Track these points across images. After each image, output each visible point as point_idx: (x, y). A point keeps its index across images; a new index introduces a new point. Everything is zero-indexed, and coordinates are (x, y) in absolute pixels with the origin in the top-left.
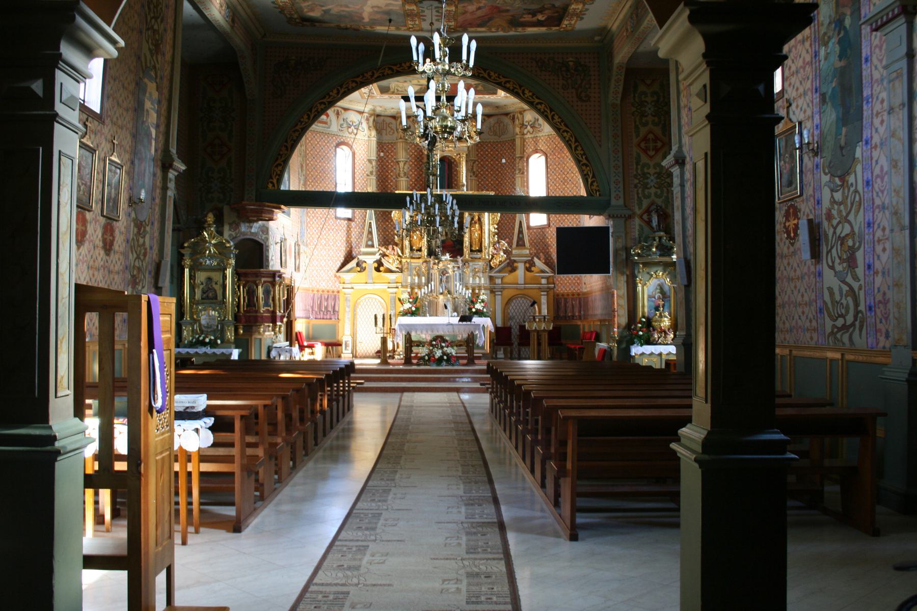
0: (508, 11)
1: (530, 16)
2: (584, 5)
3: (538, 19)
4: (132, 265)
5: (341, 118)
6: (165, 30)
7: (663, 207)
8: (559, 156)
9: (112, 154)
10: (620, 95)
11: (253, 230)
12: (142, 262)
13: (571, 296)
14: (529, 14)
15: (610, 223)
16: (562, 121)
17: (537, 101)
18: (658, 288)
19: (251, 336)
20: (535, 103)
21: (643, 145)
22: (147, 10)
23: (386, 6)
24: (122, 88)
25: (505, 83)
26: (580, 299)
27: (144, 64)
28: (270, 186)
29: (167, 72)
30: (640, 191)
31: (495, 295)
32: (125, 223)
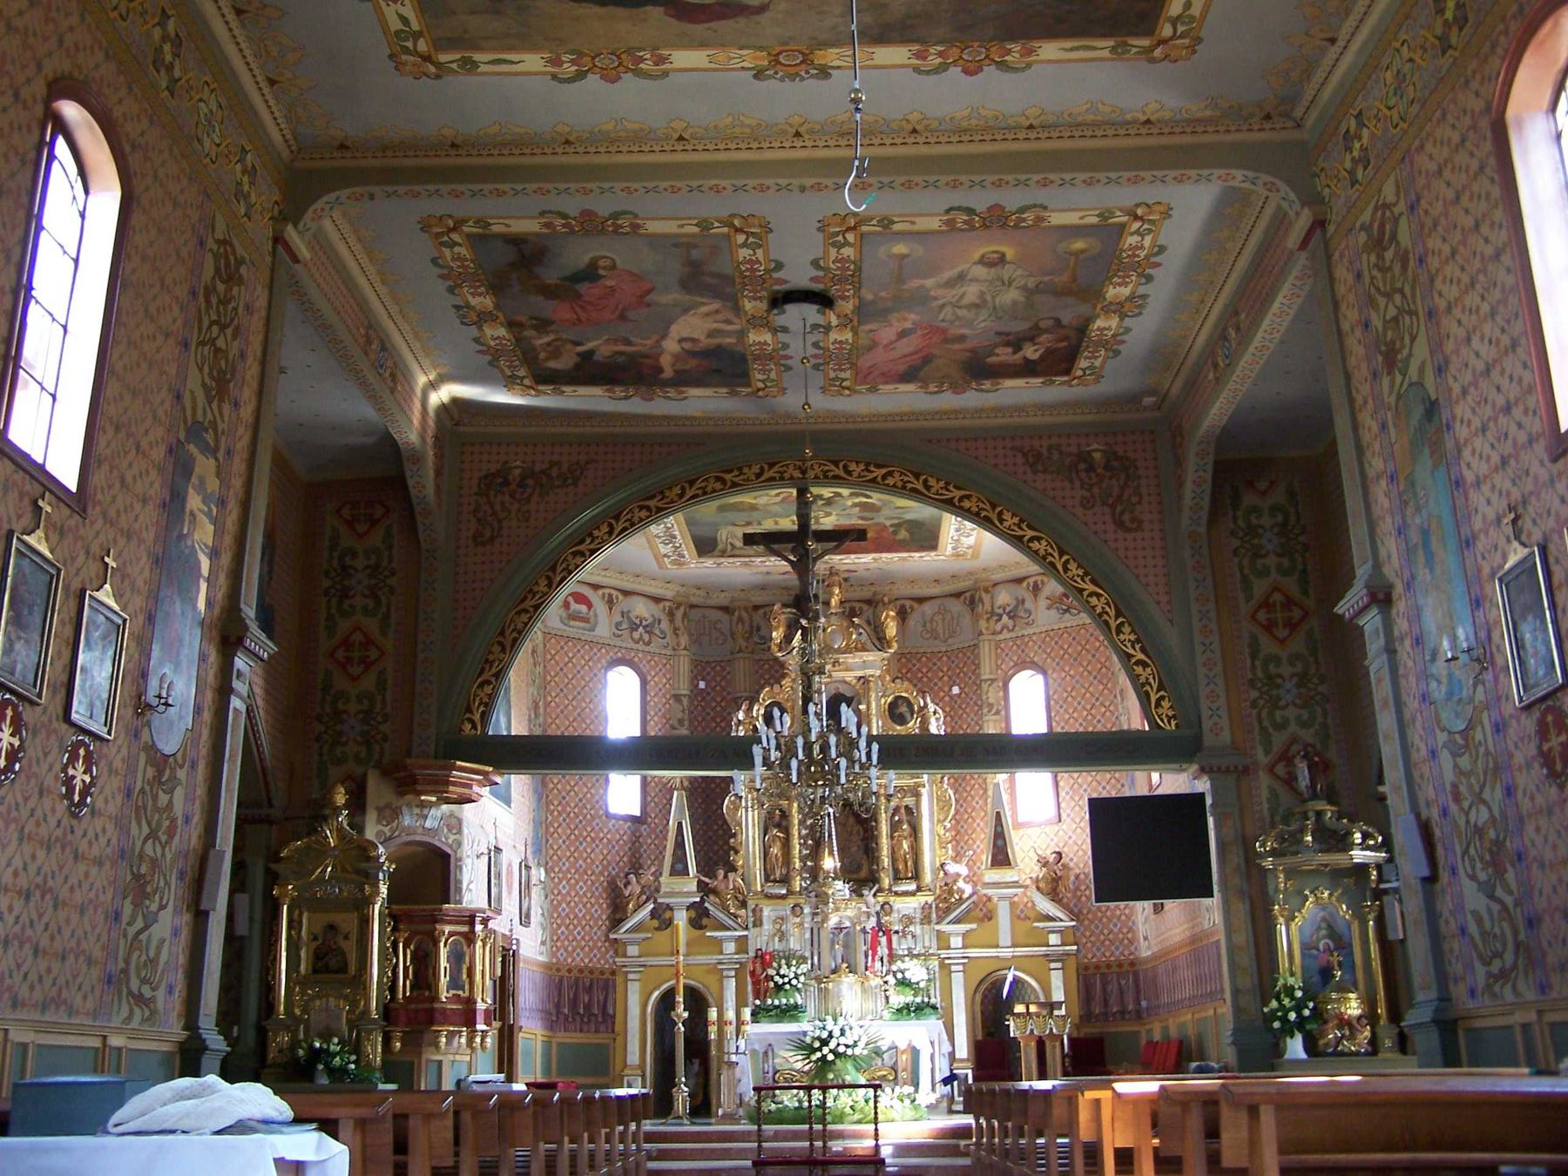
0: (962, 338)
1: (1010, 350)
2: (1122, 320)
3: (1025, 358)
4: (137, 850)
5: (617, 609)
6: (242, 355)
7: (1318, 746)
8: (1072, 672)
9: (101, 587)
10: (1205, 514)
11: (428, 824)
12: (163, 848)
13: (1115, 969)
14: (1008, 344)
15: (1203, 785)
16: (1086, 574)
17: (1030, 533)
18: (1324, 925)
19: (419, 1054)
20: (1026, 539)
21: (1262, 616)
22: (203, 305)
23: (709, 336)
24: (134, 451)
25: (961, 500)
26: (1136, 974)
27: (189, 413)
28: (468, 726)
29: (242, 444)
30: (1264, 714)
31: (951, 972)
32: (124, 751)
